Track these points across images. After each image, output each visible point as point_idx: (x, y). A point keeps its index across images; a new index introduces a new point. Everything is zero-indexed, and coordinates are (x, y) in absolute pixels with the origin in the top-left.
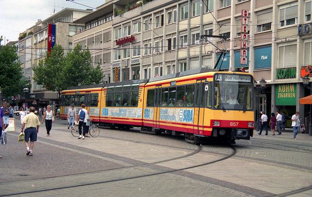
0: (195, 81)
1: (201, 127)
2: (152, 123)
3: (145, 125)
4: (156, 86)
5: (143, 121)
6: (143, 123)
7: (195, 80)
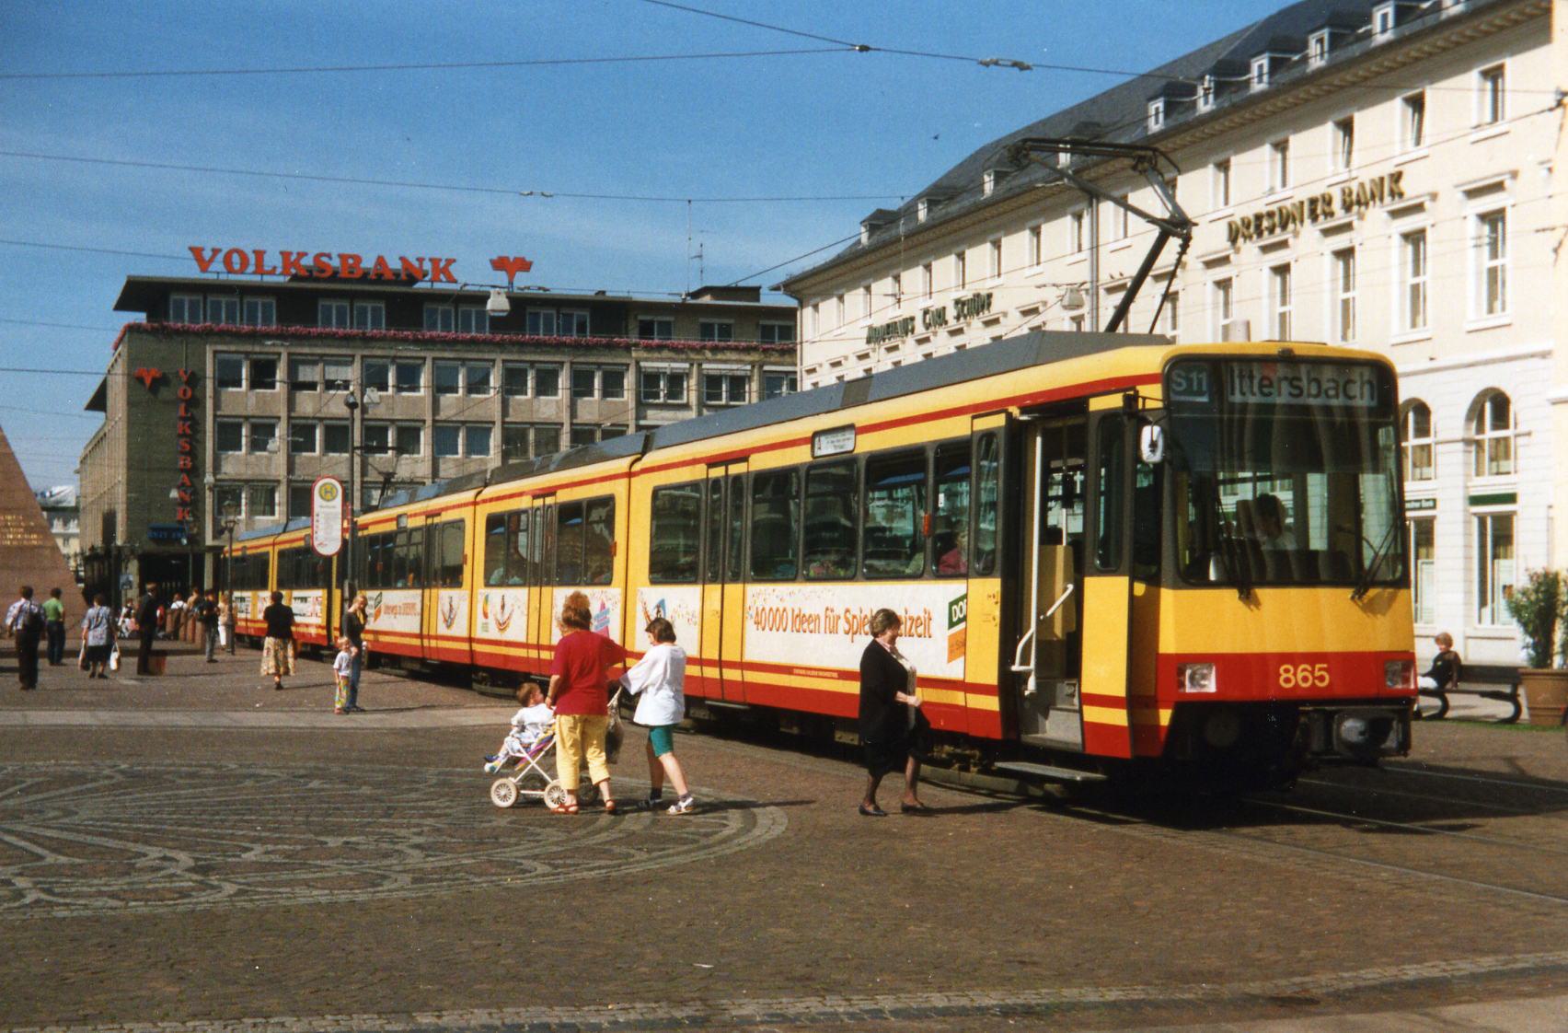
0: (699, 473)
1: (732, 665)
2: (522, 653)
3: (481, 662)
4: (535, 497)
5: (426, 643)
6: (472, 652)
7: (966, 418)
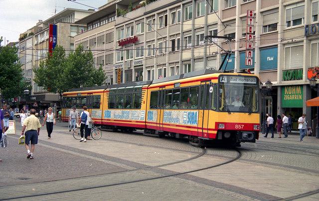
0: (199, 83)
1: (205, 129)
2: (155, 125)
3: (148, 127)
4: (160, 88)
5: (147, 124)
6: (146, 125)
7: (200, 82)
